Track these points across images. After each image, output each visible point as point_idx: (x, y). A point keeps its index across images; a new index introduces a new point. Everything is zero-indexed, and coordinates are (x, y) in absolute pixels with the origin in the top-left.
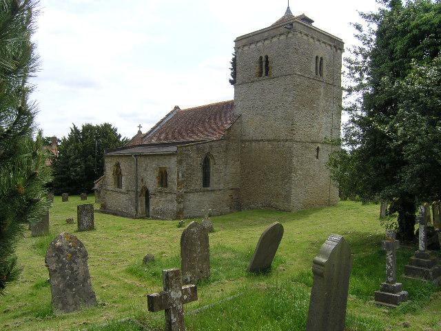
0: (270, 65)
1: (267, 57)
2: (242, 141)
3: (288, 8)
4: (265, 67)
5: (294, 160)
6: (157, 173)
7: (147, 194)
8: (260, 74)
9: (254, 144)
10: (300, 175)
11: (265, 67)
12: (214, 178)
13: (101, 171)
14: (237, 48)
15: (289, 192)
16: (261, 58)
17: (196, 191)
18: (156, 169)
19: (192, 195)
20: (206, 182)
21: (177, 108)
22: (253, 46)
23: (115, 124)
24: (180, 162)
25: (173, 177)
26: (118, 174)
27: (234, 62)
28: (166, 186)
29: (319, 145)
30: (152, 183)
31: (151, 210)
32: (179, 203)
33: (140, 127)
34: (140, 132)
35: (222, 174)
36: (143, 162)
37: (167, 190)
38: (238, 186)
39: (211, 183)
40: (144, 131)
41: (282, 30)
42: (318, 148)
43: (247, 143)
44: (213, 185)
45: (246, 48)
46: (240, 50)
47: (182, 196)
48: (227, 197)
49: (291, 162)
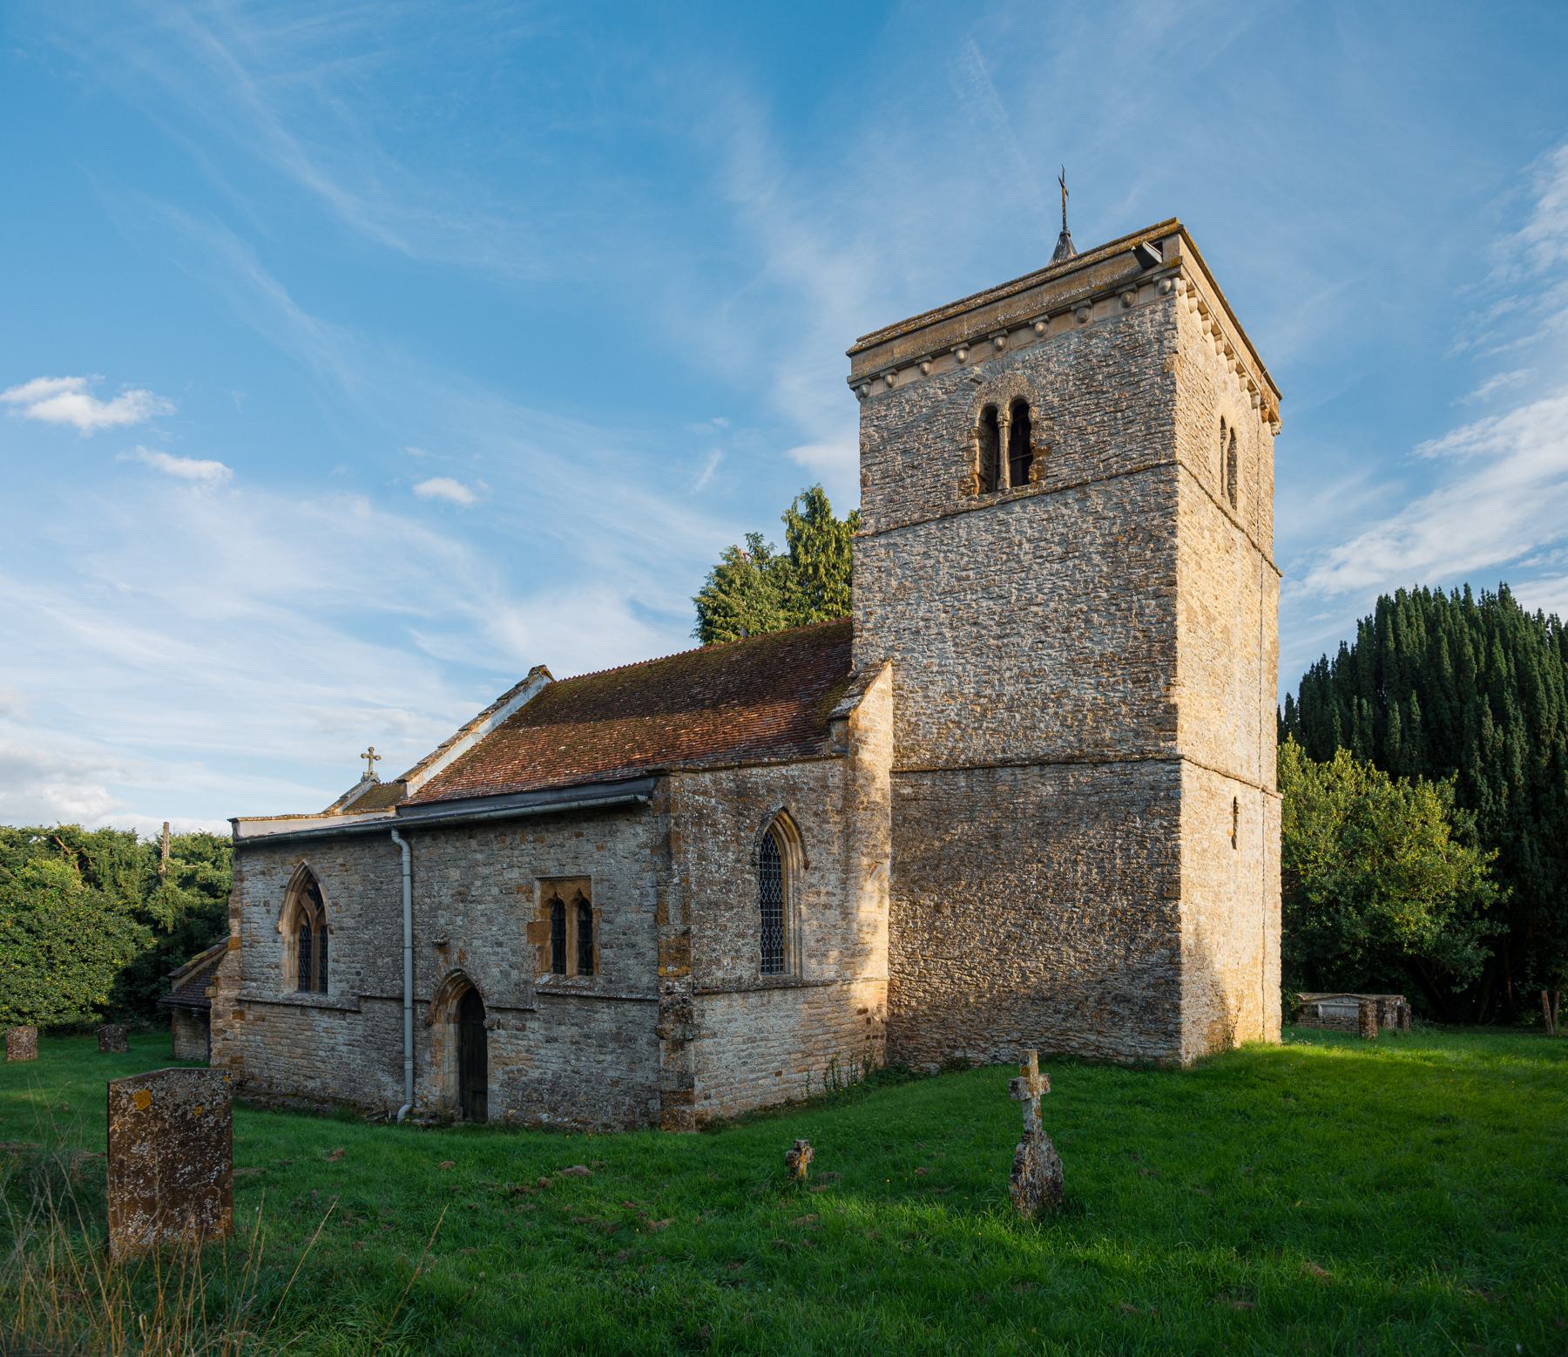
1: (1020, 408)
6: (533, 907)
8: (990, 480)
16: (991, 413)
17: (742, 989)
33: (371, 756)
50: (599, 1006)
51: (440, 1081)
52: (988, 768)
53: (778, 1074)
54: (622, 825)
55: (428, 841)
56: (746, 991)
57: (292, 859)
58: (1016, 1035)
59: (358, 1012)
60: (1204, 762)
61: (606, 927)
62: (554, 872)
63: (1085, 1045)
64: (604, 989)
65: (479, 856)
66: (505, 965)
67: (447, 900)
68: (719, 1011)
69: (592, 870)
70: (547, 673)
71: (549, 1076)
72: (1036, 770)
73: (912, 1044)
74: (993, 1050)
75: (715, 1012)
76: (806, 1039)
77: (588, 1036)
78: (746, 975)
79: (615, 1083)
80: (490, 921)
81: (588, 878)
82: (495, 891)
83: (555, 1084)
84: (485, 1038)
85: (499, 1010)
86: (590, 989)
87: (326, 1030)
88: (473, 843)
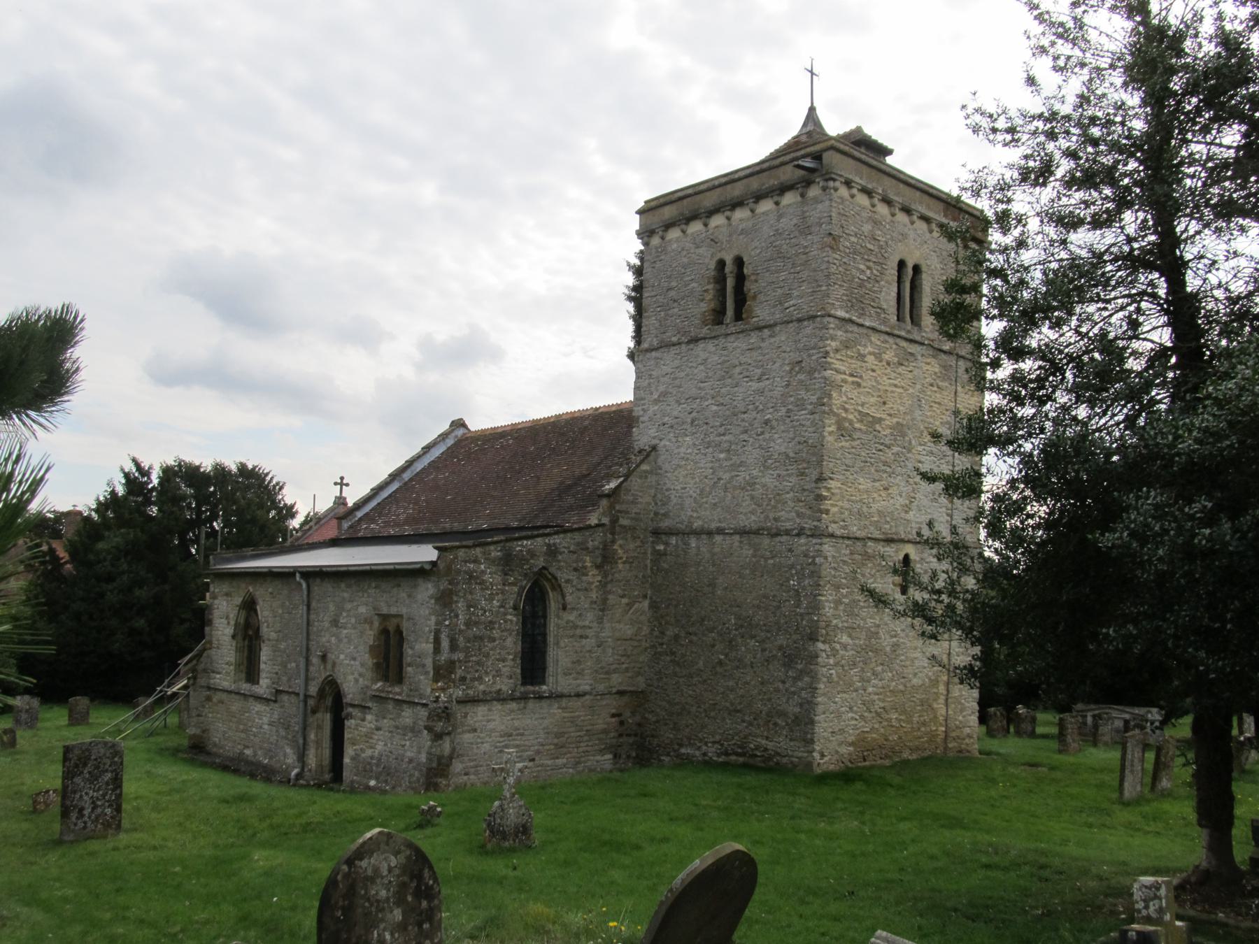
0: (747, 284)
1: (739, 262)
2: (656, 533)
3: (812, 110)
4: (732, 295)
5: (828, 597)
6: (370, 636)
7: (333, 701)
8: (718, 316)
9: (693, 542)
10: (845, 647)
11: (732, 295)
12: (559, 656)
13: (200, 621)
14: (645, 234)
15: (808, 706)
16: (721, 264)
17: (500, 698)
18: (368, 621)
19: (481, 710)
20: (533, 665)
21: (459, 424)
22: (696, 227)
23: (272, 463)
24: (445, 600)
25: (420, 648)
26: (249, 635)
27: (637, 295)
28: (400, 679)
29: (910, 549)
30: (353, 668)
31: (347, 760)
32: (438, 737)
33: (342, 483)
34: (340, 501)
35: (589, 643)
36: (330, 599)
37: (397, 691)
38: (641, 683)
39: (551, 669)
40: (353, 496)
41: (788, 174)
42: (906, 557)
43: (673, 540)
44: (558, 677)
45: (674, 234)
46: (656, 241)
47: (445, 714)
48: (603, 721)
49: (815, 607)
50: (405, 706)
51: (318, 757)
52: (710, 533)
53: (533, 760)
54: (420, 581)
55: (318, 580)
56: (504, 700)
57: (243, 586)
58: (718, 738)
59: (275, 701)
60: (859, 534)
61: (410, 652)
62: (385, 611)
63: (757, 748)
64: (408, 696)
65: (346, 595)
66: (356, 675)
67: (327, 624)
68: (480, 714)
69: (404, 611)
70: (464, 425)
71: (376, 754)
72: (737, 537)
73: (656, 741)
74: (704, 748)
75: (479, 714)
76: (559, 735)
77: (397, 727)
78: (504, 688)
79: (411, 761)
80: (349, 642)
81: (401, 616)
82: (353, 620)
83: (379, 760)
84: (343, 725)
85: (353, 706)
86: (400, 694)
87: (257, 712)
88: (343, 585)
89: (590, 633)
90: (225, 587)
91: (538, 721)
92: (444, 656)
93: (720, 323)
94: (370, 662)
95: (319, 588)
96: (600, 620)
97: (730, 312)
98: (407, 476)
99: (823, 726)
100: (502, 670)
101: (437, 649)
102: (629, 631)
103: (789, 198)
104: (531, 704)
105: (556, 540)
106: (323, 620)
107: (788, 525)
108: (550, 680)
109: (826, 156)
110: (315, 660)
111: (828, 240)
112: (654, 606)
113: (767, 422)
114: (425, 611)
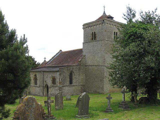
2: (86, 66)
4: (94, 37)
7: (47, 87)
9: (90, 67)
12: (74, 81)
14: (84, 28)
15: (103, 86)
16: (93, 32)
20: (71, 82)
21: (61, 51)
22: (90, 28)
24: (60, 74)
25: (57, 80)
26: (36, 79)
31: (49, 94)
33: (45, 58)
34: (45, 61)
40: (47, 60)
44: (74, 84)
46: (85, 29)
47: (61, 88)
49: (104, 74)
89: (78, 78)
90: (32, 73)
91: (72, 89)
92: (60, 81)
93: (93, 40)
94: (51, 82)
95: (44, 73)
96: (79, 77)
97: (94, 39)
98: (54, 58)
99: (105, 88)
100: (68, 83)
101: (60, 80)
102: (82, 78)
103: (100, 25)
104: (71, 87)
105: (73, 67)
106: (45, 77)
107: (101, 65)
108: (73, 84)
109: (104, 20)
110: (44, 82)
111: (105, 30)
112: (85, 75)
113: (98, 52)
114: (58, 76)
